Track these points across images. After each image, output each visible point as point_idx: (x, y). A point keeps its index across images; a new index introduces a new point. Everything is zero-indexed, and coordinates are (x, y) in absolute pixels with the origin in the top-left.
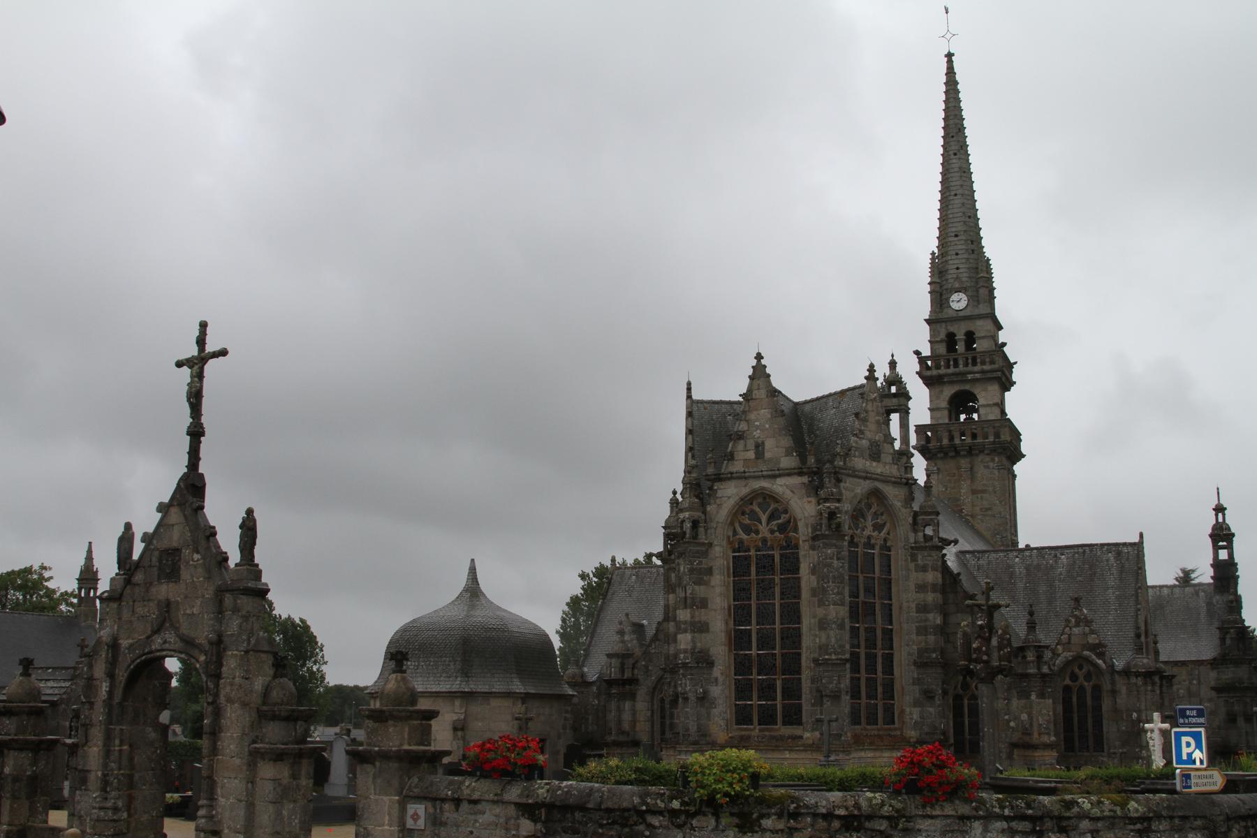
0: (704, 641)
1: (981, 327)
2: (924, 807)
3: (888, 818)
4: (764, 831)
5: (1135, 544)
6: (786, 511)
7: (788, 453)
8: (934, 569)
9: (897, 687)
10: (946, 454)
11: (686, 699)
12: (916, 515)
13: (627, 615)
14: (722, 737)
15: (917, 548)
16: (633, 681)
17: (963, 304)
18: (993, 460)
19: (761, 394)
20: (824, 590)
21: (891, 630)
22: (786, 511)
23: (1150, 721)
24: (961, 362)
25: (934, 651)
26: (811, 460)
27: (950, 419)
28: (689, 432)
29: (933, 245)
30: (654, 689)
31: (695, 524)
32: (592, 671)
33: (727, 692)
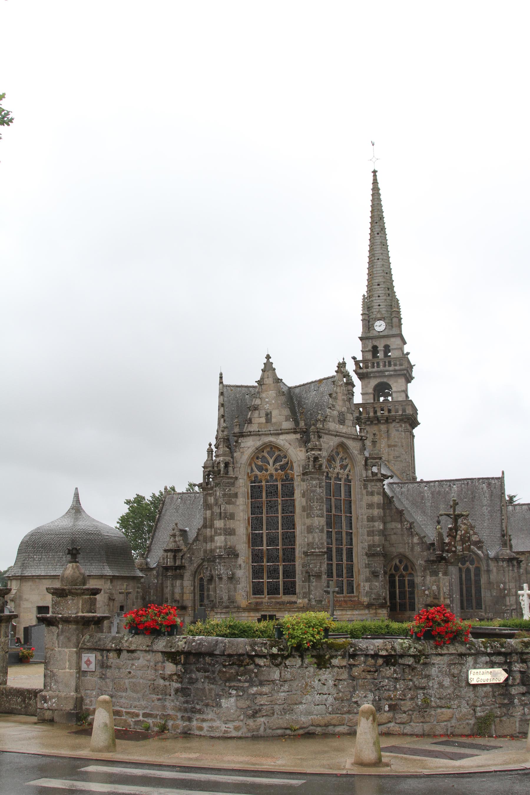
0: (232, 540)
1: (394, 342)
2: (436, 648)
3: (414, 656)
4: (334, 666)
5: (499, 478)
6: (285, 457)
7: (287, 420)
8: (378, 494)
9: (355, 569)
10: (372, 422)
11: (221, 579)
12: (366, 459)
13: (176, 524)
14: (244, 603)
15: (368, 481)
16: (182, 567)
17: (382, 328)
18: (401, 426)
19: (269, 381)
20: (311, 508)
21: (351, 533)
22: (285, 457)
23: (522, 589)
24: (381, 364)
25: (379, 546)
26: (302, 424)
27: (374, 401)
28: (222, 405)
29: (364, 290)
30: (196, 572)
31: (227, 465)
32: (153, 562)
33: (247, 574)
